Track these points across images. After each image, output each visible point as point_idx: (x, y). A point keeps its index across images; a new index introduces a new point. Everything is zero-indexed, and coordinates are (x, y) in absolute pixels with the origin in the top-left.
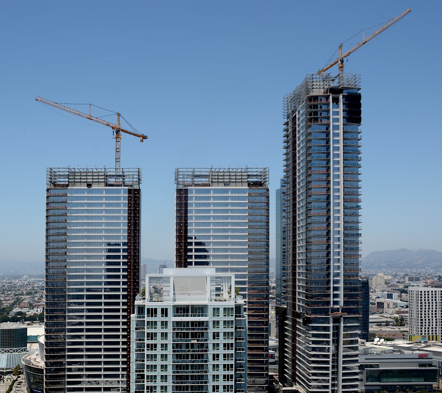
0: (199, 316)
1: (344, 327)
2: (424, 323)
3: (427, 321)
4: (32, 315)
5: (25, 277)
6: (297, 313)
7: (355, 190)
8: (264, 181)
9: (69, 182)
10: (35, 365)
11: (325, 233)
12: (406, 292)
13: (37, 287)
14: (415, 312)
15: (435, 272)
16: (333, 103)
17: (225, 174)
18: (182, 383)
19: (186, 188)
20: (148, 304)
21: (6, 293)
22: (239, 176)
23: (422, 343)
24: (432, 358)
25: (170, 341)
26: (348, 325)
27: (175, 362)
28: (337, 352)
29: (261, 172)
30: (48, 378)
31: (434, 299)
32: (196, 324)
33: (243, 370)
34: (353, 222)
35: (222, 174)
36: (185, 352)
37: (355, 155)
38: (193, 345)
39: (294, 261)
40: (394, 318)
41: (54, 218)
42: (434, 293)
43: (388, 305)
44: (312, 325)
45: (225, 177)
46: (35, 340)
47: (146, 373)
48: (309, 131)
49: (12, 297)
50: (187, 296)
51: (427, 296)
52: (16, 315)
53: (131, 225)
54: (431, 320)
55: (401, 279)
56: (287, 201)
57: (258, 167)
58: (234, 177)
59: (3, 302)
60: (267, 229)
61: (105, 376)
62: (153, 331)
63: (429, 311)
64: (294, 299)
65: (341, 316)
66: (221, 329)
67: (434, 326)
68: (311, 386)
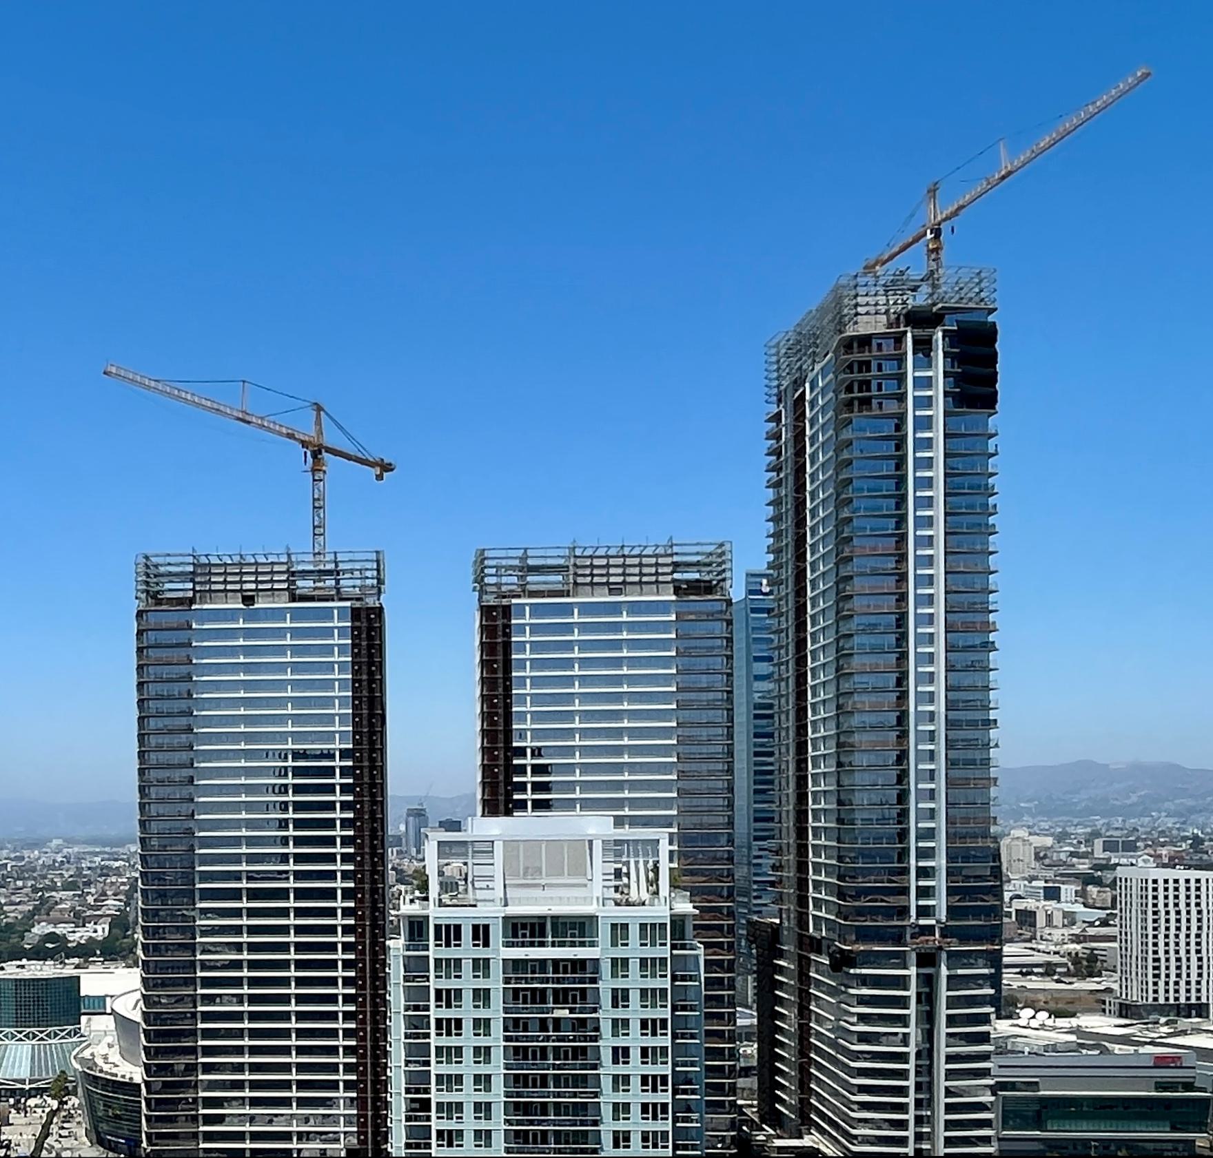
0: (573, 944)
1: (949, 977)
2: (1163, 968)
3: (1173, 963)
4: (83, 942)
5: (56, 842)
6: (812, 938)
7: (978, 598)
8: (720, 577)
9: (193, 589)
10: (107, 1073)
11: (892, 718)
12: (1098, 882)
13: (89, 868)
14: (1136, 939)
15: (1178, 826)
16: (914, 353)
17: (612, 561)
18: (531, 1123)
19: (505, 602)
20: (436, 914)
21: (12, 885)
22: (650, 566)
23: (1162, 1025)
24: (1194, 1068)
25: (496, 1012)
26: (960, 972)
27: (510, 1066)
28: (928, 1046)
29: (711, 554)
30: (153, 1107)
31: (1193, 901)
32: (565, 967)
33: (693, 1092)
34: (973, 688)
35: (604, 562)
36: (538, 1041)
37: (979, 500)
38: (557, 1021)
39: (802, 797)
40: (1070, 954)
41: (159, 686)
42: (1193, 885)
43: (1049, 917)
44: (858, 971)
45: (612, 571)
46: (98, 1005)
47: (435, 1097)
48: (847, 434)
49: (27, 895)
50: (538, 892)
51: (1171, 893)
52: (41, 943)
53: (361, 703)
54: (1184, 960)
55: (1082, 846)
56: (779, 631)
57: (703, 541)
58: (636, 570)
59: (5, 908)
60: (728, 710)
61: (302, 1102)
62: (452, 984)
63: (1177, 936)
64: (802, 901)
65: (940, 948)
66: (634, 981)
67: (1194, 978)
68: (855, 1137)
